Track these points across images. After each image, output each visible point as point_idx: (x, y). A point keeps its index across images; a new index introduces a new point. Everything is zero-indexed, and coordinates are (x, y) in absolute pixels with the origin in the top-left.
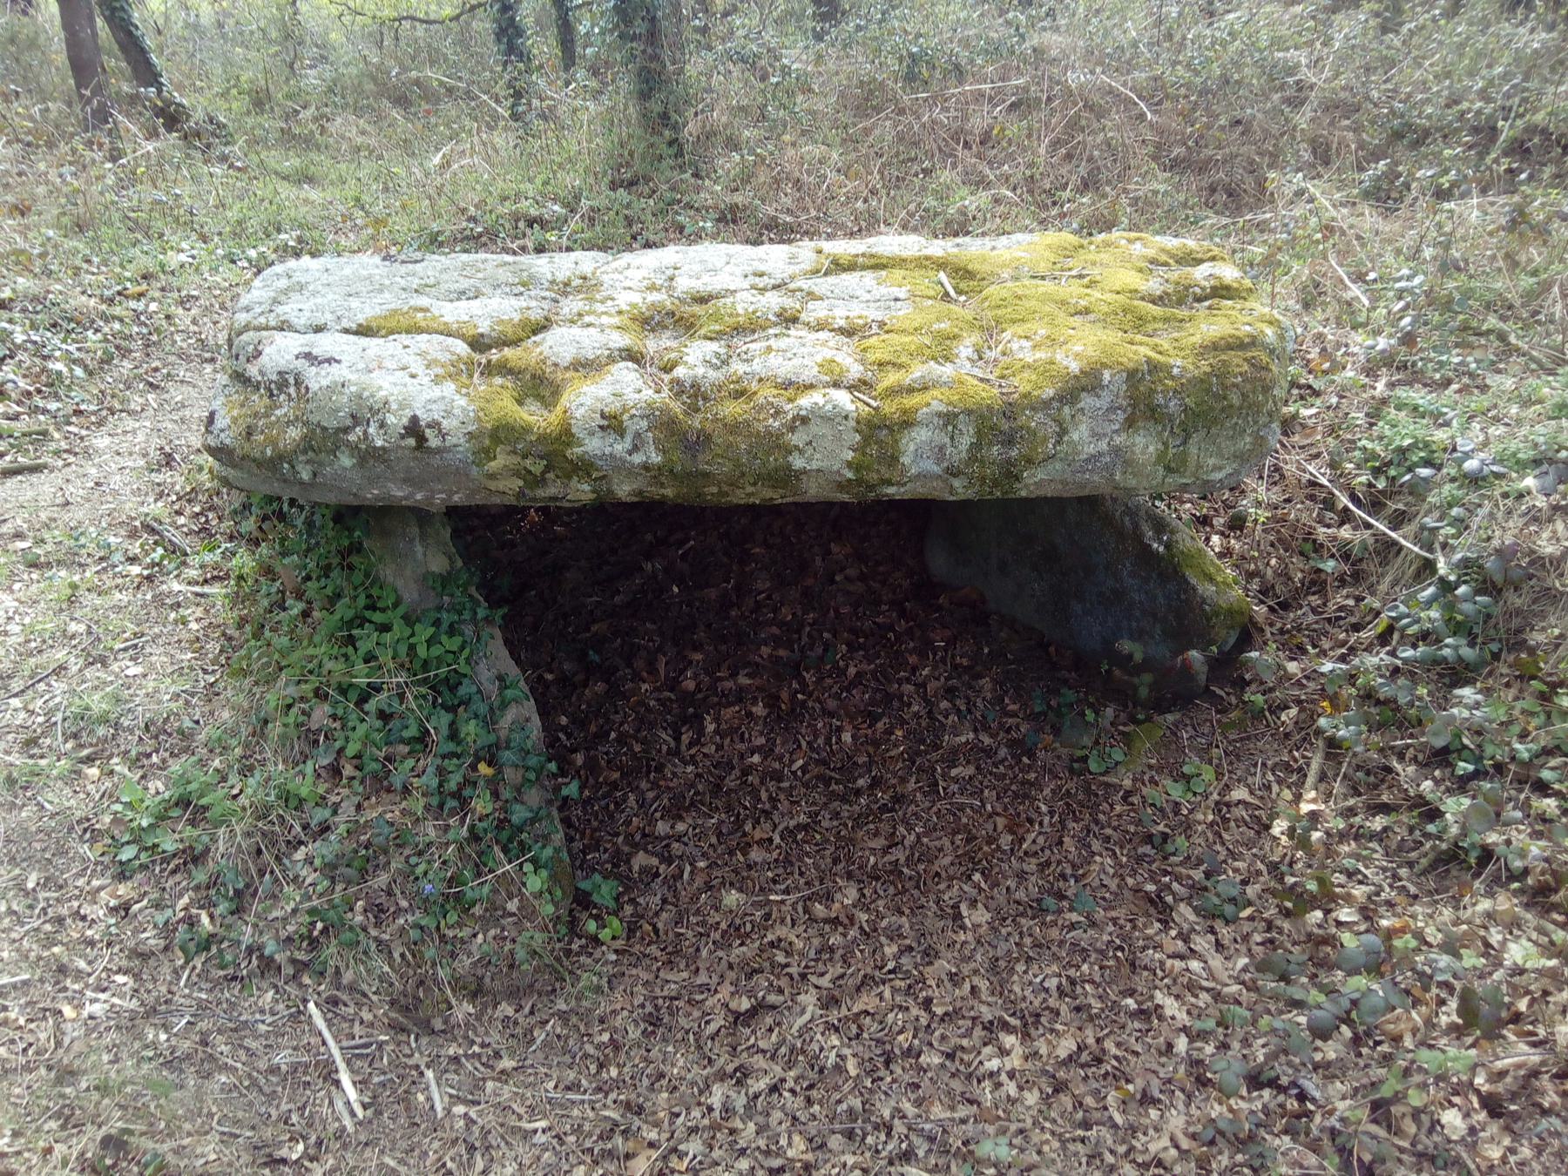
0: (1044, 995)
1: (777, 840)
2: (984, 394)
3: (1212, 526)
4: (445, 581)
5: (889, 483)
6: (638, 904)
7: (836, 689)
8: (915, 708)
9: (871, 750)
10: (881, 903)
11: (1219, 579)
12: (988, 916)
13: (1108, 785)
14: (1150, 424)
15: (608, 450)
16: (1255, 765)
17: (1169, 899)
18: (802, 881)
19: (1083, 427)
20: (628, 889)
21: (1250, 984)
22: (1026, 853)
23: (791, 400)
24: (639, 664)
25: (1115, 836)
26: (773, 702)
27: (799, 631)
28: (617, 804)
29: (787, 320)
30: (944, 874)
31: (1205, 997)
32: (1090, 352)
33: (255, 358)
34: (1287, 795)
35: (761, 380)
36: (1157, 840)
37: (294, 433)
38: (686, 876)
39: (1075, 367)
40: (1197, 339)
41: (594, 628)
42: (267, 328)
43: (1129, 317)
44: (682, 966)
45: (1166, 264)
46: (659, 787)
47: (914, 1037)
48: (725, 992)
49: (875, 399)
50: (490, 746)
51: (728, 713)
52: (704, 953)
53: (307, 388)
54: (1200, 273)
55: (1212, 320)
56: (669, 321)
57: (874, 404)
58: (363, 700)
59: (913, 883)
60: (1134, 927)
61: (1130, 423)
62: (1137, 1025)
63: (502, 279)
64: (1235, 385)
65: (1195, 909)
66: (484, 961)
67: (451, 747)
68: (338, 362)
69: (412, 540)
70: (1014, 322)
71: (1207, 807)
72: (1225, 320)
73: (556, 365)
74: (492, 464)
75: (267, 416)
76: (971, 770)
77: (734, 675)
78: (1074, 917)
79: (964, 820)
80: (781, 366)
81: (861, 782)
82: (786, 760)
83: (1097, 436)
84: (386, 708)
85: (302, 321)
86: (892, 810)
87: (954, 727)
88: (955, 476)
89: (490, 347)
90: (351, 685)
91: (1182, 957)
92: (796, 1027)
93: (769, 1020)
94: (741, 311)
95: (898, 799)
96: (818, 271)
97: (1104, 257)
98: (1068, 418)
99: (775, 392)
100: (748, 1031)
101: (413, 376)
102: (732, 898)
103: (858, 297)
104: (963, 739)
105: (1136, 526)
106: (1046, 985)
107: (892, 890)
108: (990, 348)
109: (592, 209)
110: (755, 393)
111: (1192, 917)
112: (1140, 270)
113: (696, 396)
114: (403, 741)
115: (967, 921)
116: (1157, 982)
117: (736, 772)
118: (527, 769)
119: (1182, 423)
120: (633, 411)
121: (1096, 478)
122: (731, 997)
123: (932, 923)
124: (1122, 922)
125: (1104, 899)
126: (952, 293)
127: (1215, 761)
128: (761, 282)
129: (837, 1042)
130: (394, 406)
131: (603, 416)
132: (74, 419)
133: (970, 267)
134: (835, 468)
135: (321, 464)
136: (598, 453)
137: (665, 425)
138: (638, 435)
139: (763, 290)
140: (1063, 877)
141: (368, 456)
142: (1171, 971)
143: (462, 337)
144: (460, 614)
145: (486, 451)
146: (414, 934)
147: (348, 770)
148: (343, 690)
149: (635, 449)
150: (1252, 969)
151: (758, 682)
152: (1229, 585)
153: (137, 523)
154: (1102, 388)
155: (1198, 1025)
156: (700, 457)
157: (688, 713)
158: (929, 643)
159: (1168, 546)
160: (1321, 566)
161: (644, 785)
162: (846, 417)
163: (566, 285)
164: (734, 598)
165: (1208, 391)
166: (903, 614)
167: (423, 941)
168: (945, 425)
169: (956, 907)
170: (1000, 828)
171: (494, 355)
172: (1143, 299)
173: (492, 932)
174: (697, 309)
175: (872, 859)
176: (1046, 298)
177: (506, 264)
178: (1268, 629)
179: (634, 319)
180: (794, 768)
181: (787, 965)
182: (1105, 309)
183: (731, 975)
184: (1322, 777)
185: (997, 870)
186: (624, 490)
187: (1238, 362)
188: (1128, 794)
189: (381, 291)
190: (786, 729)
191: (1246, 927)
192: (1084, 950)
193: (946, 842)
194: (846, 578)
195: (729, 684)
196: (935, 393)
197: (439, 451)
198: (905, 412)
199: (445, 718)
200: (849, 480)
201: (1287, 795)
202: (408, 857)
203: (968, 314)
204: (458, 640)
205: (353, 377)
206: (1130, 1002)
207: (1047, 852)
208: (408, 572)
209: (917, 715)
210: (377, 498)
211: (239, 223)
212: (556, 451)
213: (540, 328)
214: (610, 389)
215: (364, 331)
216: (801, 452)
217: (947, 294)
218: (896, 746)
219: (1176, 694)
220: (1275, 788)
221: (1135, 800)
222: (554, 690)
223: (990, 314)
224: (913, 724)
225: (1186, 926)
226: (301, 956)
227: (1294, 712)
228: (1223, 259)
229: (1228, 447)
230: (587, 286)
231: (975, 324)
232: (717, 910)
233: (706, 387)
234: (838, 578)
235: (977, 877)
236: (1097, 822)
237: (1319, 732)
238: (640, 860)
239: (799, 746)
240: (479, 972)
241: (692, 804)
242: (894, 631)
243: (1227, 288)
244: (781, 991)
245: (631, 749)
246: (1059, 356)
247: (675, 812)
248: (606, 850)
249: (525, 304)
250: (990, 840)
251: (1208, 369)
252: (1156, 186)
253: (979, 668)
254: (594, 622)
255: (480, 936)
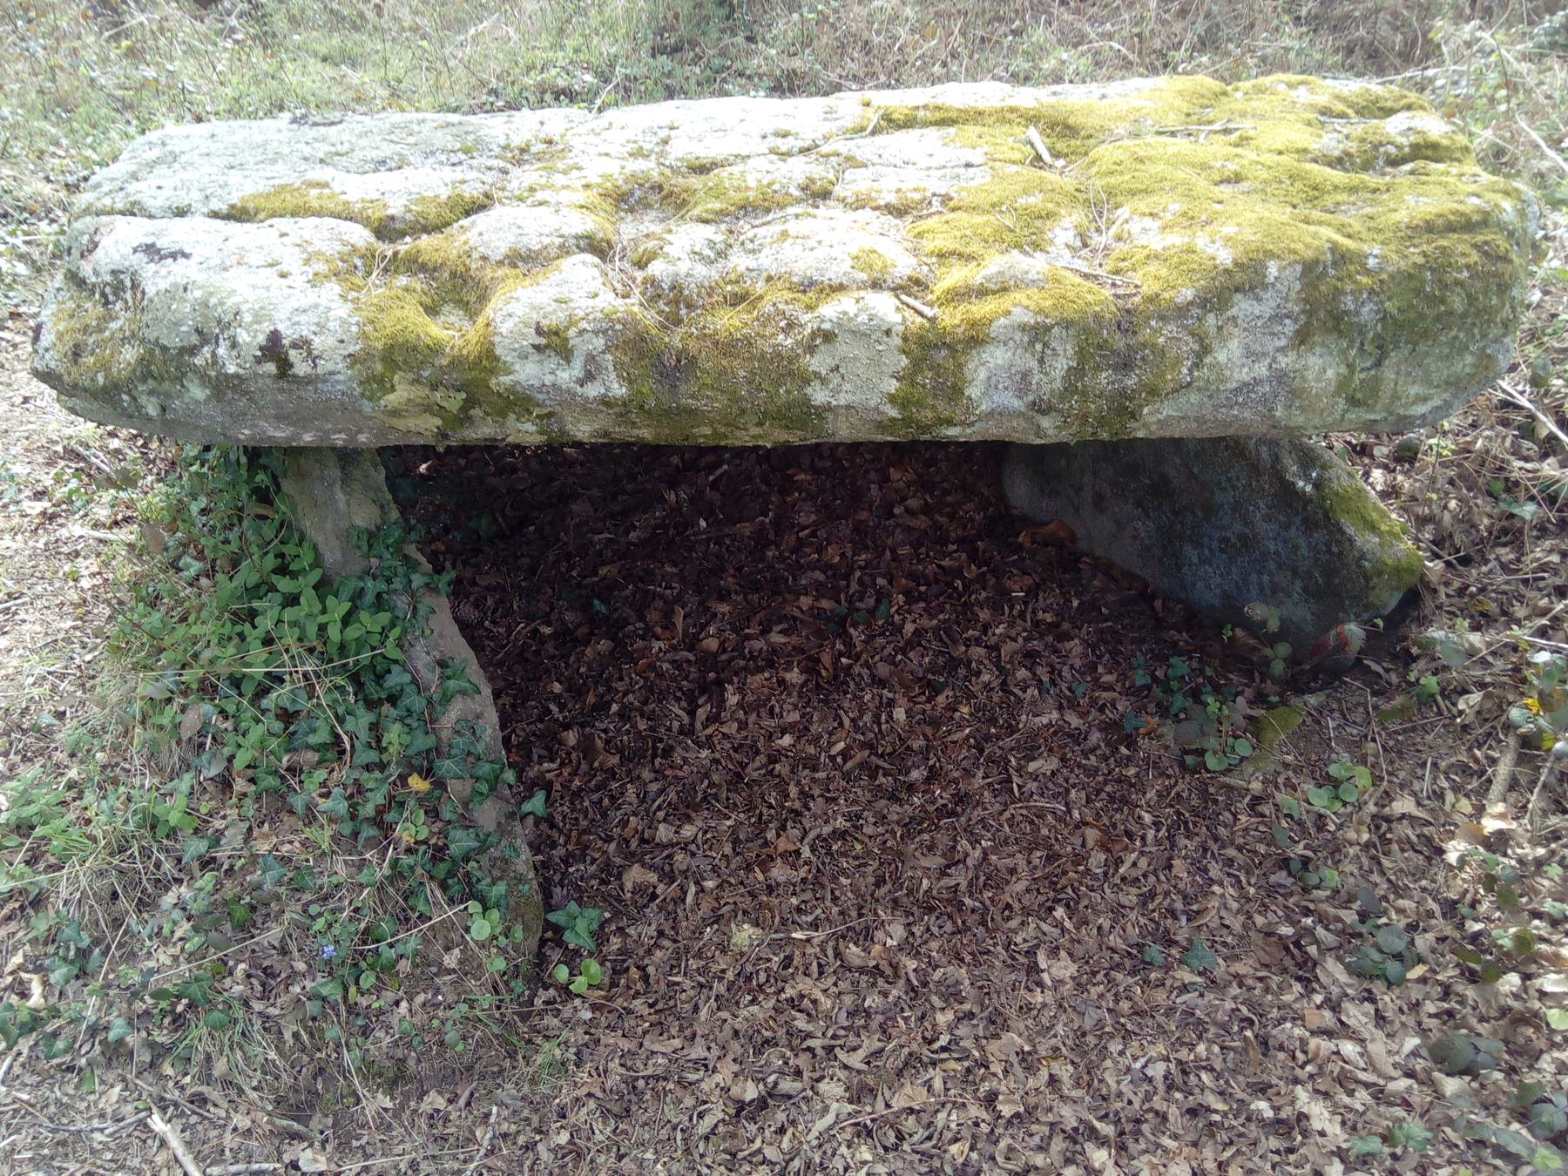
0: (1145, 1087)
1: (806, 852)
2: (1090, 298)
3: (1372, 457)
4: (372, 536)
5: (950, 422)
6: (628, 935)
7: (889, 649)
8: (986, 677)
9: (929, 731)
10: (934, 945)
11: (1384, 528)
12: (1073, 969)
13: (1230, 788)
14: (1331, 339)
15: (548, 379)
16: (1424, 764)
17: (1312, 950)
18: (835, 910)
19: (1234, 344)
20: (617, 914)
21: (1422, 1076)
22: (1123, 879)
23: (809, 308)
24: (653, 616)
25: (1241, 859)
26: (811, 666)
27: (847, 577)
28: (613, 798)
29: (815, 195)
30: (1016, 906)
31: (1363, 1095)
32: (1248, 235)
33: (90, 252)
34: (1465, 806)
35: (769, 279)
36: (1295, 866)
37: (130, 354)
38: (689, 899)
39: (1225, 257)
40: (1402, 216)
41: (603, 571)
42: (111, 212)
43: (1299, 185)
44: (674, 1031)
45: (1342, 115)
46: (665, 777)
47: (972, 1149)
48: (726, 1071)
49: (931, 305)
50: (428, 751)
51: (755, 681)
52: (704, 1013)
53: (143, 293)
54: (1394, 127)
55: (1421, 189)
56: (654, 198)
57: (929, 312)
58: (262, 692)
59: (976, 917)
60: (1267, 990)
61: (1302, 338)
62: (1274, 1143)
63: (439, 144)
64: (1457, 283)
65: (1349, 968)
66: (404, 1041)
67: (373, 756)
68: (186, 256)
69: (331, 485)
70: (1133, 193)
71: (1361, 823)
72: (1439, 190)
73: (484, 258)
74: (391, 397)
75: (100, 330)
76: (1054, 763)
77: (765, 632)
78: (1186, 976)
79: (1045, 831)
80: (800, 261)
81: (915, 775)
82: (824, 742)
83: (1252, 355)
84: (288, 706)
85: (159, 202)
86: (953, 814)
87: (1033, 703)
88: (1043, 412)
89: (403, 234)
90: (244, 675)
91: (1328, 1033)
92: (814, 1133)
93: (781, 1117)
94: (752, 183)
95: (961, 799)
96: (863, 129)
97: (1259, 104)
98: (1213, 331)
99: (788, 295)
100: (753, 1128)
101: (283, 275)
102: (744, 935)
103: (917, 161)
104: (1045, 720)
105: (1276, 458)
106: (1149, 1072)
107: (949, 927)
108: (1098, 230)
109: (627, 77)
110: (761, 297)
111: (1343, 977)
112: (1309, 124)
113: (677, 303)
114: (309, 747)
115: (1045, 977)
116: (1298, 1071)
117: (762, 759)
118: (478, 779)
119: (1378, 336)
120: (584, 325)
121: (1247, 414)
122: (728, 1080)
123: (1001, 977)
124: (1250, 982)
125: (1225, 944)
126: (1046, 157)
127: (1371, 759)
128: (784, 145)
129: (868, 1156)
130: (247, 318)
131: (539, 331)
132: (10, 323)
133: (1071, 121)
134: (872, 403)
135: (168, 395)
136: (536, 383)
137: (633, 346)
138: (591, 358)
139: (785, 155)
140: (1173, 914)
141: (223, 386)
142: (1316, 1055)
143: (366, 222)
144: (389, 581)
145: (380, 380)
146: (312, 1008)
147: (240, 785)
148: (236, 682)
149: (589, 377)
150: (1424, 1052)
151: (794, 640)
152: (1397, 537)
153: (59, 448)
154: (1265, 287)
155: (1359, 1146)
156: (683, 388)
157: (708, 682)
158: (1004, 593)
159: (1317, 485)
160: (1516, 511)
161: (647, 774)
162: (888, 333)
163: (523, 151)
164: (772, 536)
165: (1418, 292)
166: (973, 556)
167: (325, 1015)
168: (1032, 343)
169: (1031, 953)
170: (1090, 843)
171: (405, 246)
172: (1315, 161)
173: (420, 998)
174: (695, 181)
175: (925, 882)
176: (1178, 161)
177: (448, 125)
178: (1442, 590)
179: (605, 196)
180: (834, 751)
181: (809, 1035)
182: (1264, 174)
183: (736, 1047)
184: (1513, 785)
185: (1085, 902)
186: (583, 430)
187: (1463, 249)
188: (1257, 800)
189: (274, 161)
190: (826, 702)
191: (1416, 993)
192: (1200, 1022)
193: (1020, 860)
194: (908, 511)
195: (759, 644)
196: (1019, 296)
197: (309, 380)
198: (973, 325)
199: (365, 718)
200: (893, 420)
201: (1465, 806)
202: (307, 904)
203: (1068, 183)
204: (385, 617)
205: (200, 277)
206: (1263, 1107)
207: (1152, 879)
208: (329, 526)
209: (987, 687)
210: (252, 438)
211: (236, 100)
212: (475, 377)
213: (473, 208)
214: (554, 292)
215: (238, 215)
216: (824, 382)
217: (1039, 158)
218: (960, 727)
219: (1318, 669)
220: (1450, 797)
221: (1266, 809)
222: (550, 647)
223: (1099, 183)
224: (983, 698)
225: (1335, 990)
226: (162, 1037)
227: (1476, 697)
228: (1422, 108)
229: (1440, 370)
230: (550, 151)
231: (1078, 197)
232: (724, 952)
233: (691, 290)
234: (897, 511)
235: (1060, 912)
236: (1216, 839)
237: (1509, 727)
238: (635, 875)
239: (841, 724)
240: (399, 1053)
241: (704, 799)
242: (963, 578)
243: (1434, 146)
244: (798, 1073)
245: (634, 726)
246: (1201, 241)
247: (681, 812)
248: (594, 861)
249: (459, 176)
250: (1079, 859)
251: (1420, 260)
252: (1288, 42)
253: (1066, 626)
254: (603, 564)
255: (404, 1004)
